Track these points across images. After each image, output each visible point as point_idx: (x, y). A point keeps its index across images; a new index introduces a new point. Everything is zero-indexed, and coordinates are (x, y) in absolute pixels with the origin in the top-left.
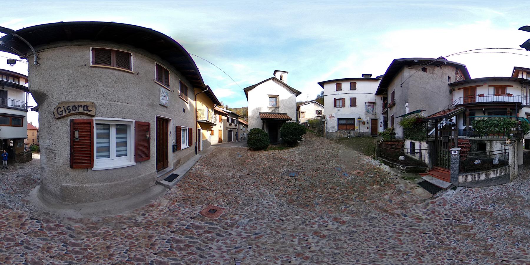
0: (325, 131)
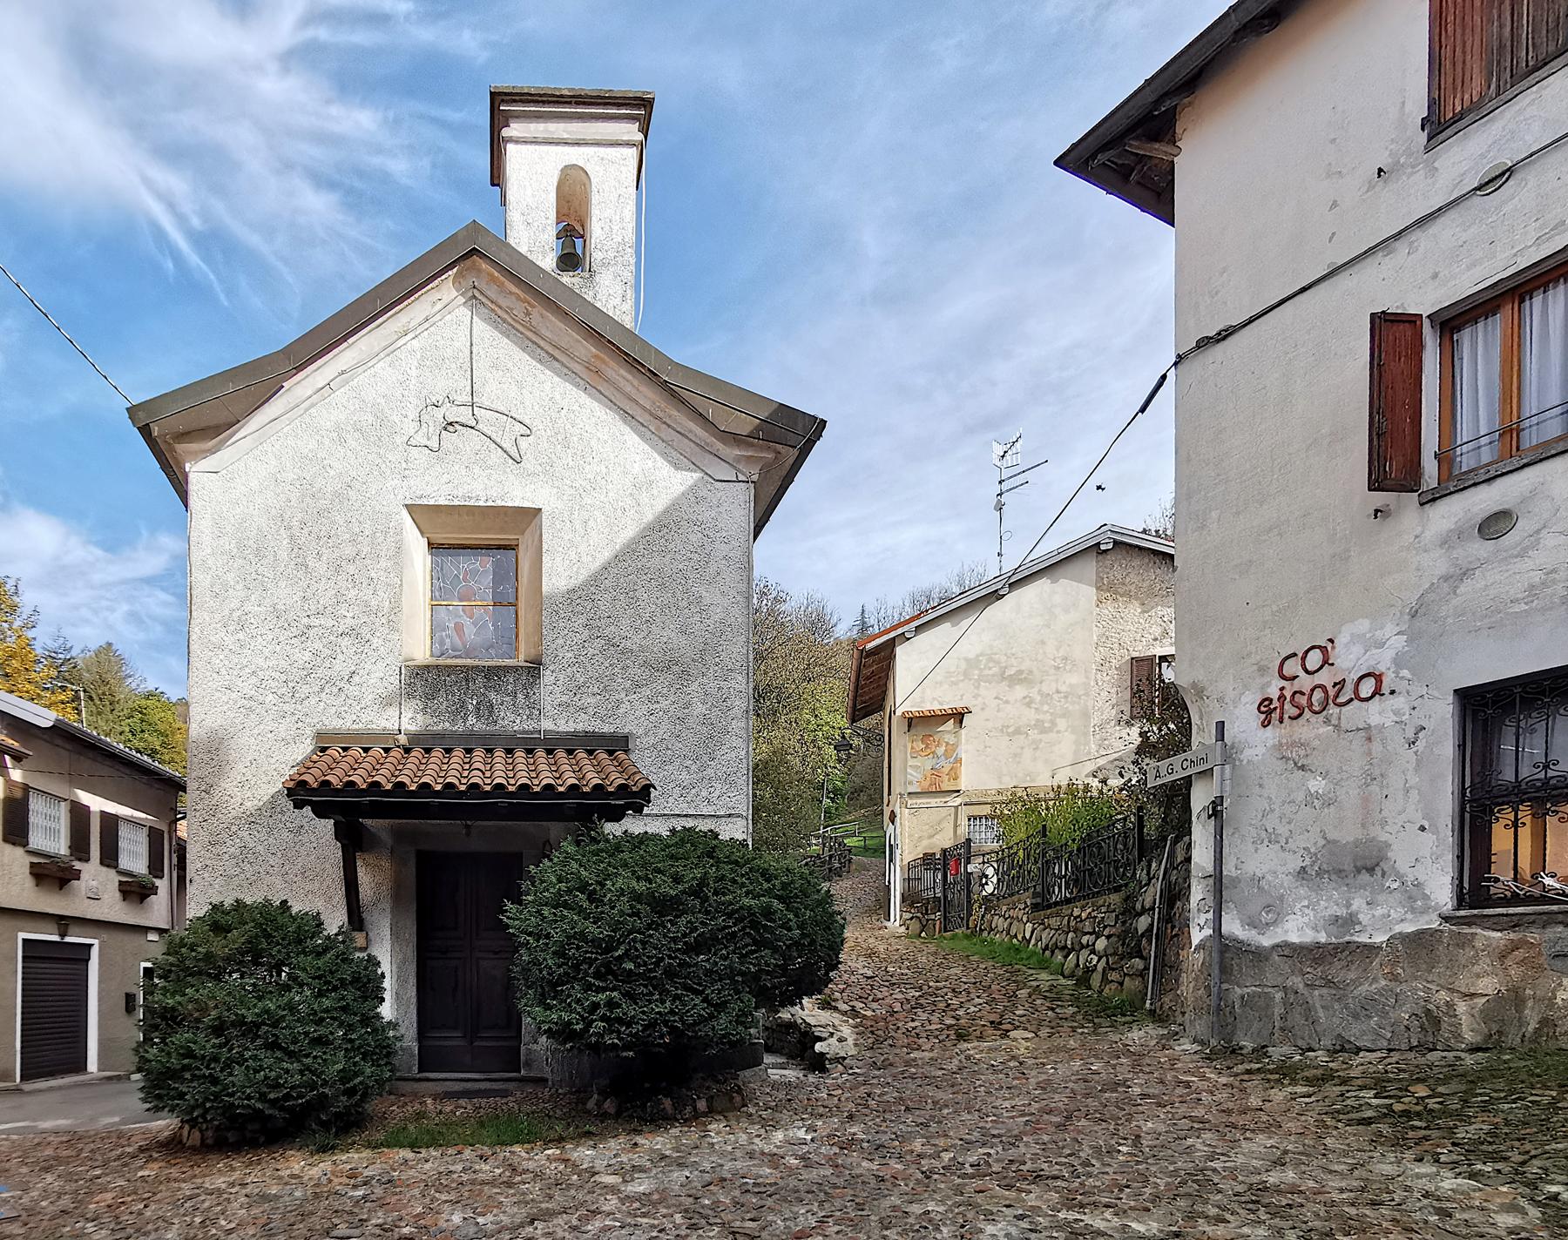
0: (1197, 937)
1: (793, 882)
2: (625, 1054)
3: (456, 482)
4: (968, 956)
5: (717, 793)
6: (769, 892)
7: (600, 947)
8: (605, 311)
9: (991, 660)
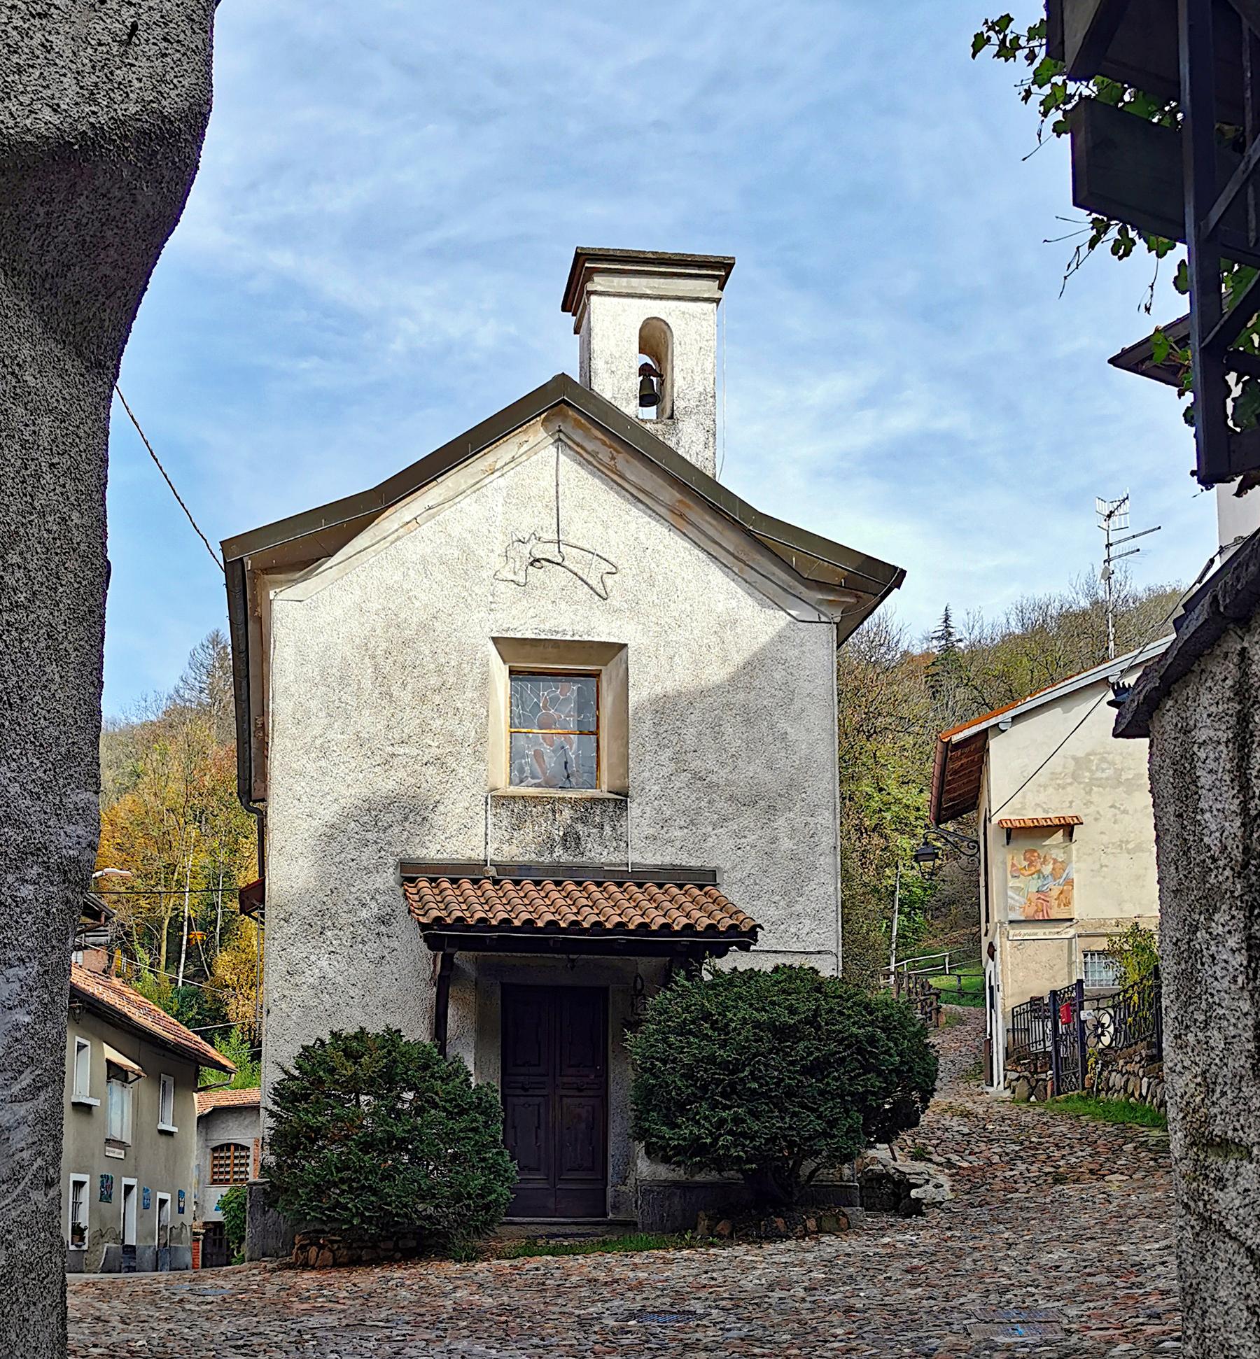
1: (892, 1015)
2: (748, 1166)
3: (542, 616)
4: (1078, 1116)
5: (806, 930)
6: (872, 1023)
7: (728, 1069)
8: (688, 459)
9: (1103, 760)
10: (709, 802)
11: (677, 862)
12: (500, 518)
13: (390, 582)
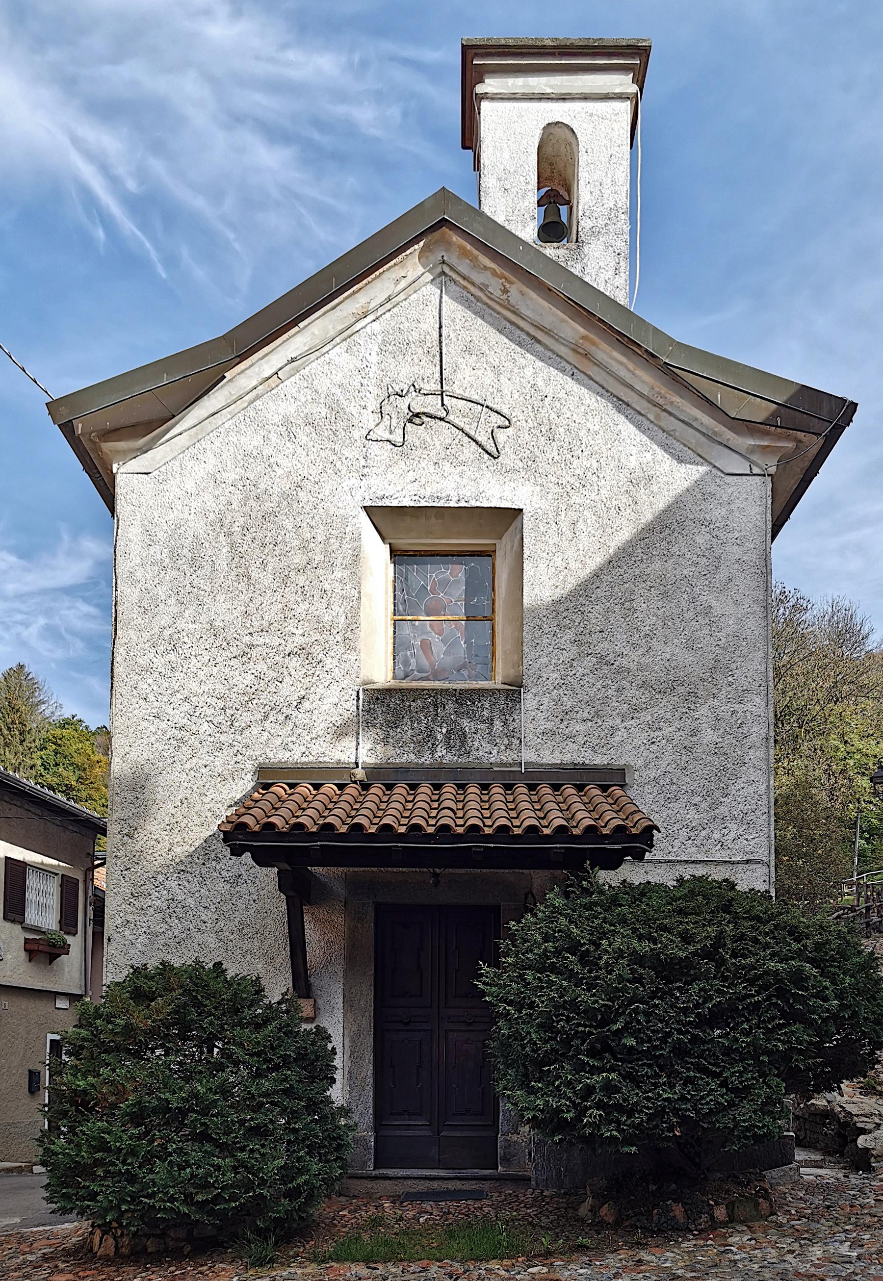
1: (828, 942)
5: (732, 835)
10: (618, 690)
11: (580, 760)
12: (374, 368)
13: (249, 448)
